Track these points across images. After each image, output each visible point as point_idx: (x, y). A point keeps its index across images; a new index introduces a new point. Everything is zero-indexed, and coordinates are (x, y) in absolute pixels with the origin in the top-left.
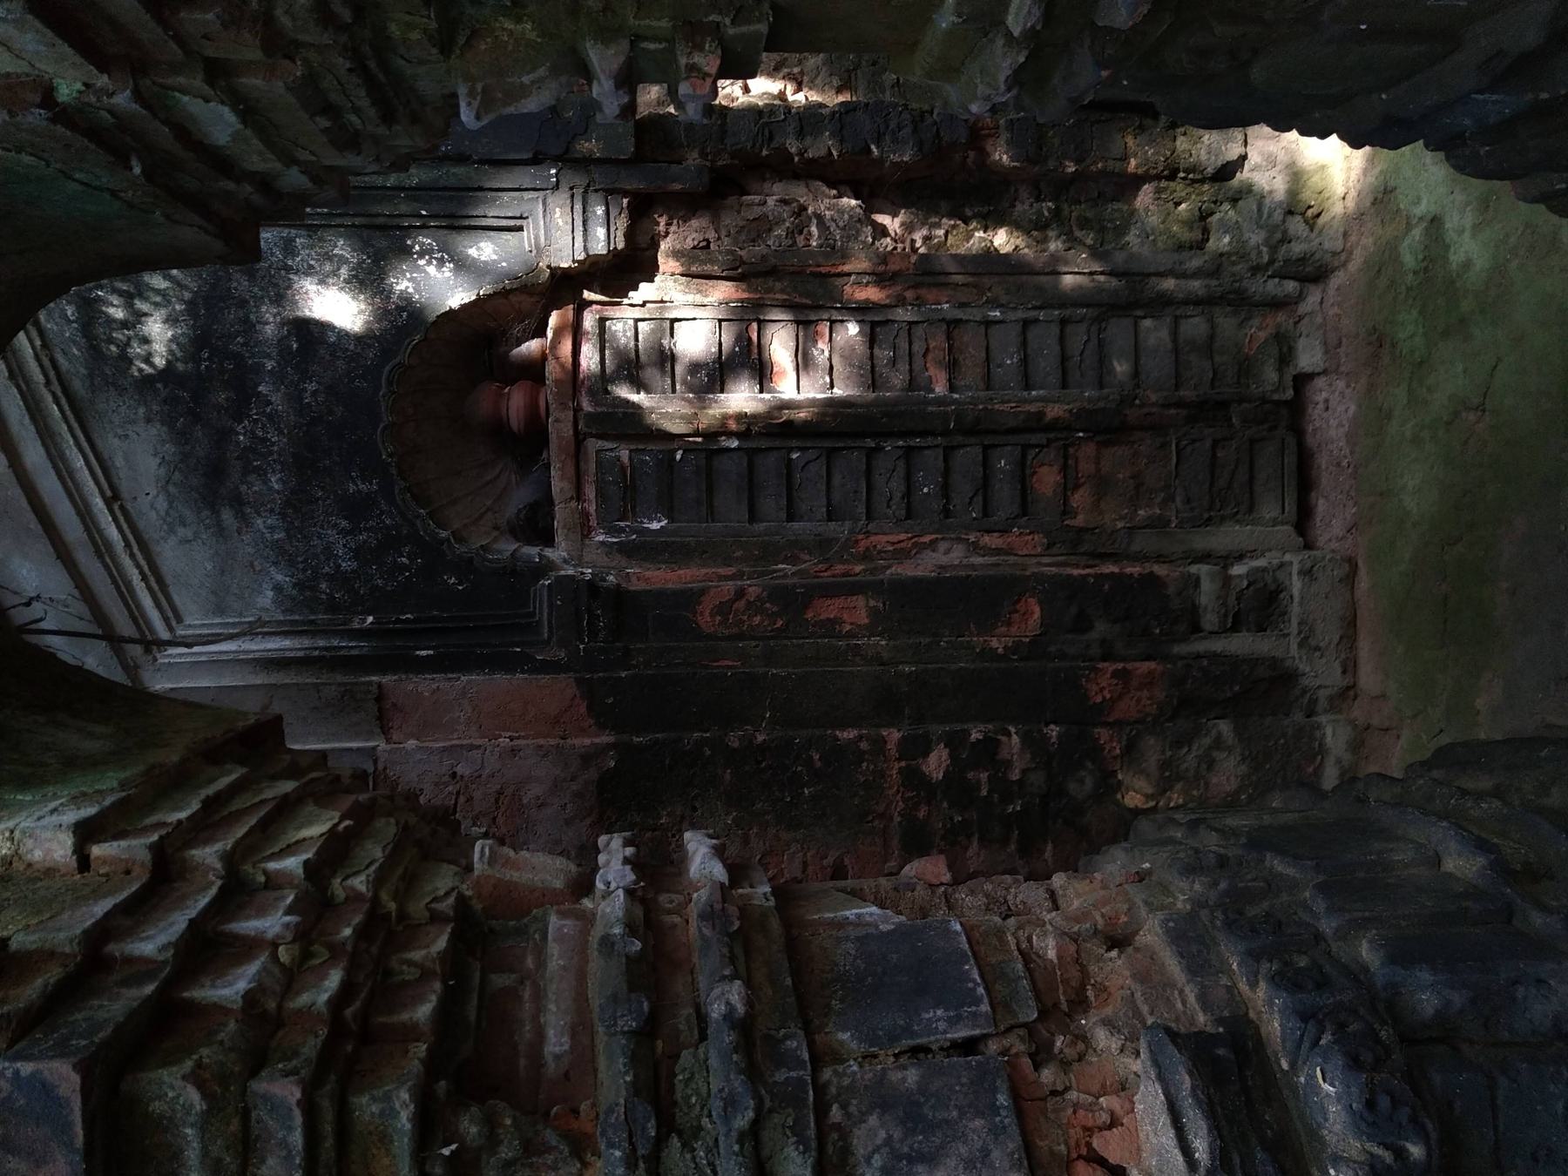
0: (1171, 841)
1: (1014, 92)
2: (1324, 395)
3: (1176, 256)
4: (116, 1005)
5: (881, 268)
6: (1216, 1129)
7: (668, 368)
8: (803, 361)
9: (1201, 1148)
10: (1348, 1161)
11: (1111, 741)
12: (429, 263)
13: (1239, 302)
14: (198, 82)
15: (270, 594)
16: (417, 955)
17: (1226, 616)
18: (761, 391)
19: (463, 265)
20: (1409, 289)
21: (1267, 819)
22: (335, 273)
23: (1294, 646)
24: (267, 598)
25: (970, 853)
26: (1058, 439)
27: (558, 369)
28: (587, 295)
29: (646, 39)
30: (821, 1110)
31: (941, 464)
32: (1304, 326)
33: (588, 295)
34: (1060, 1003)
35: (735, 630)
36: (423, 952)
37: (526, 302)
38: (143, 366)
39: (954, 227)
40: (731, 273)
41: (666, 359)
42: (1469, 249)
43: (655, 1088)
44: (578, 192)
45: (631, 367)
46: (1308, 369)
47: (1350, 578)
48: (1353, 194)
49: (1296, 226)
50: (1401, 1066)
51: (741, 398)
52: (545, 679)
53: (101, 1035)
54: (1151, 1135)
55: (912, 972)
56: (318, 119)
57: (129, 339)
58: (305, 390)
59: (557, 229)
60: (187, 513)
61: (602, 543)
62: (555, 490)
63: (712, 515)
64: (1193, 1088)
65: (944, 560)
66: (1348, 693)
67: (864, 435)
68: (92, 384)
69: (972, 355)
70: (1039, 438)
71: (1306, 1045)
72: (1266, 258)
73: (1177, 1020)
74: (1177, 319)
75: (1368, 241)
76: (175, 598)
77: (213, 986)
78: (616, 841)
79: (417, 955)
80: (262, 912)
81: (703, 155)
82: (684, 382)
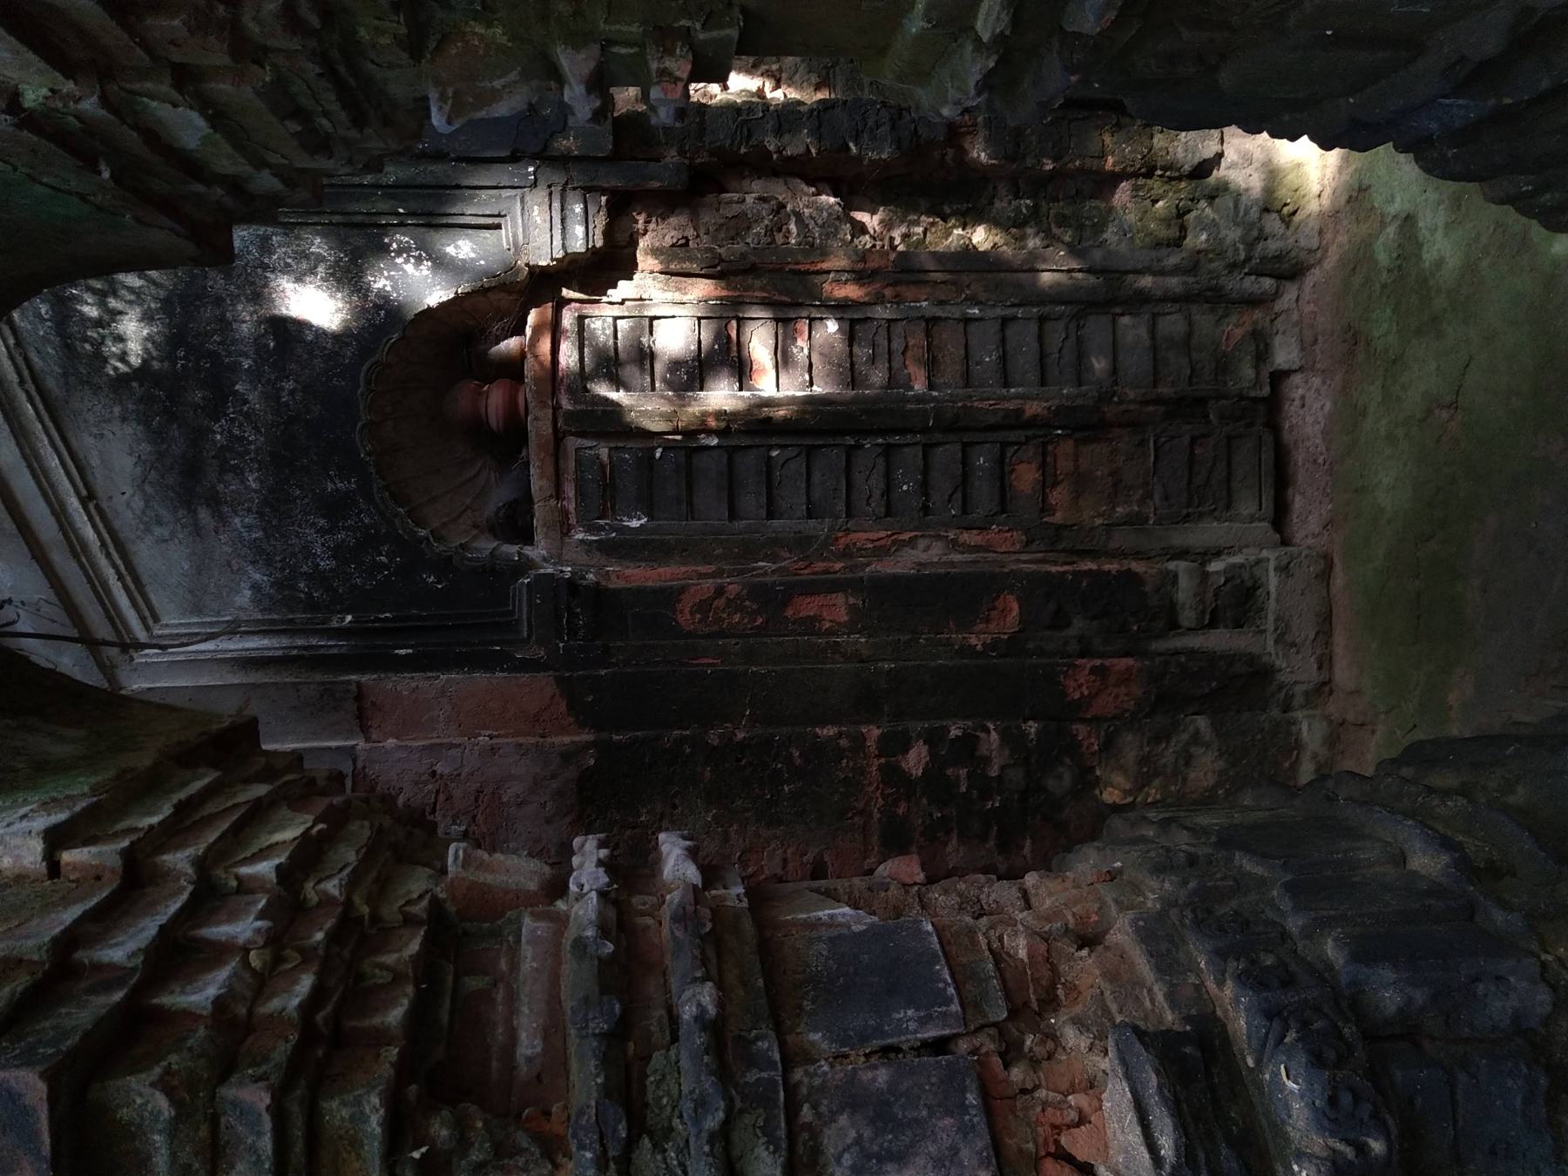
0: (1144, 840)
1: (985, 95)
2: (1300, 391)
3: (1154, 254)
4: (84, 1013)
5: (860, 266)
6: (1181, 1126)
7: (648, 366)
8: (783, 359)
9: (1167, 1145)
10: (1311, 1157)
11: (1089, 736)
12: (407, 261)
13: (1216, 299)
14: (165, 88)
15: (248, 593)
16: (390, 959)
17: (1203, 612)
18: (741, 389)
19: (441, 264)
20: (1384, 286)
21: (1238, 817)
22: (312, 271)
23: (1271, 643)
24: (244, 597)
25: (949, 849)
26: (1035, 437)
27: (537, 367)
28: (565, 292)
29: (617, 43)
30: (792, 1110)
31: (920, 462)
32: (1279, 324)
33: (567, 293)
34: (1031, 1002)
35: (715, 628)
36: (395, 956)
37: (504, 300)
38: (119, 365)
39: (933, 224)
40: (711, 271)
41: (645, 356)
42: (1441, 247)
43: (626, 1090)
44: (556, 190)
45: (610, 365)
46: (1285, 367)
47: (1326, 575)
48: (1328, 192)
49: (1273, 223)
50: (1365, 1061)
51: (721, 396)
52: (525, 678)
53: (69, 1043)
54: (1119, 1132)
55: (884, 972)
56: (287, 123)
57: (103, 337)
58: (282, 389)
59: (536, 226)
60: (163, 512)
61: (582, 541)
62: (534, 487)
63: (691, 513)
64: (1160, 1087)
65: (924, 557)
66: (1323, 688)
67: (843, 433)
68: (67, 383)
69: (951, 352)
70: (1013, 436)
71: (1271, 1042)
72: (1242, 257)
73: (1146, 1018)
74: (1154, 316)
75: (1342, 238)
76: (152, 597)
77: (183, 992)
78: (591, 843)
79: (390, 959)
80: (233, 917)
81: (681, 152)
82: (664, 380)
